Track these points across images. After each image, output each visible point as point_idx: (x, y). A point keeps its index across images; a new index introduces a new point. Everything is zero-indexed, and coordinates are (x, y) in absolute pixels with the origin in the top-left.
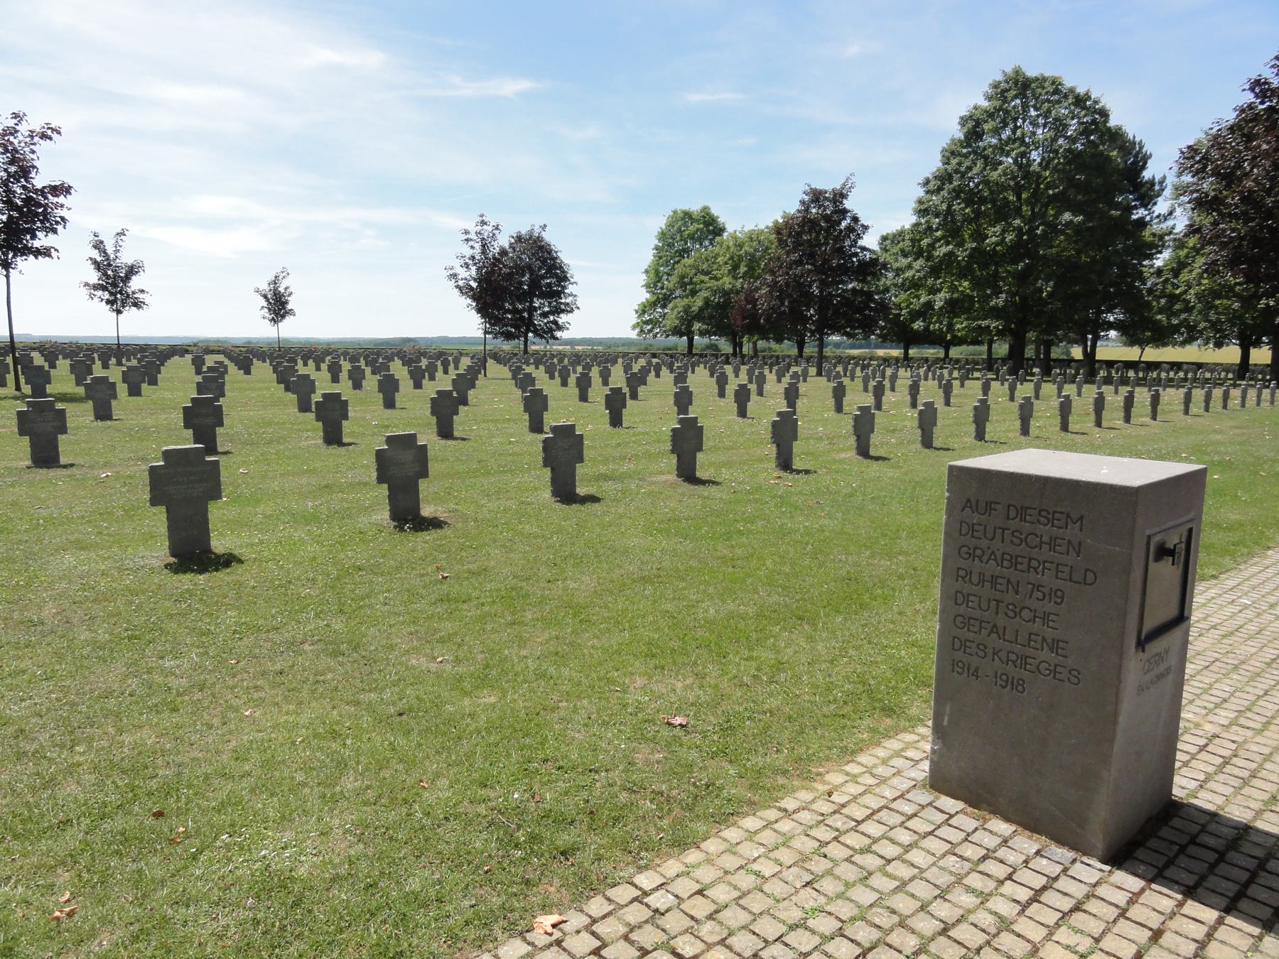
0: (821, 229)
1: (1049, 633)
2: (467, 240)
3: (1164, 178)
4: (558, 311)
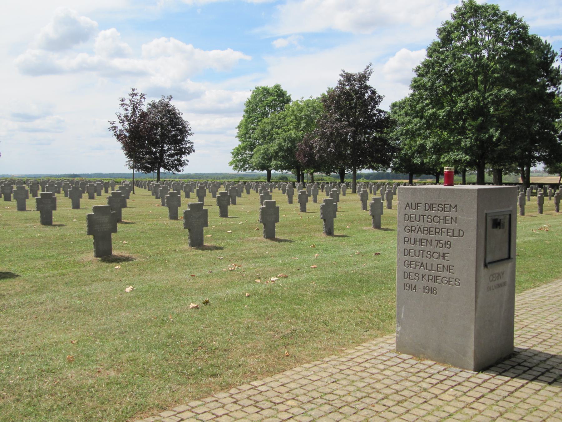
0: (353, 98)
1: (446, 263)
2: (122, 105)
4: (182, 152)
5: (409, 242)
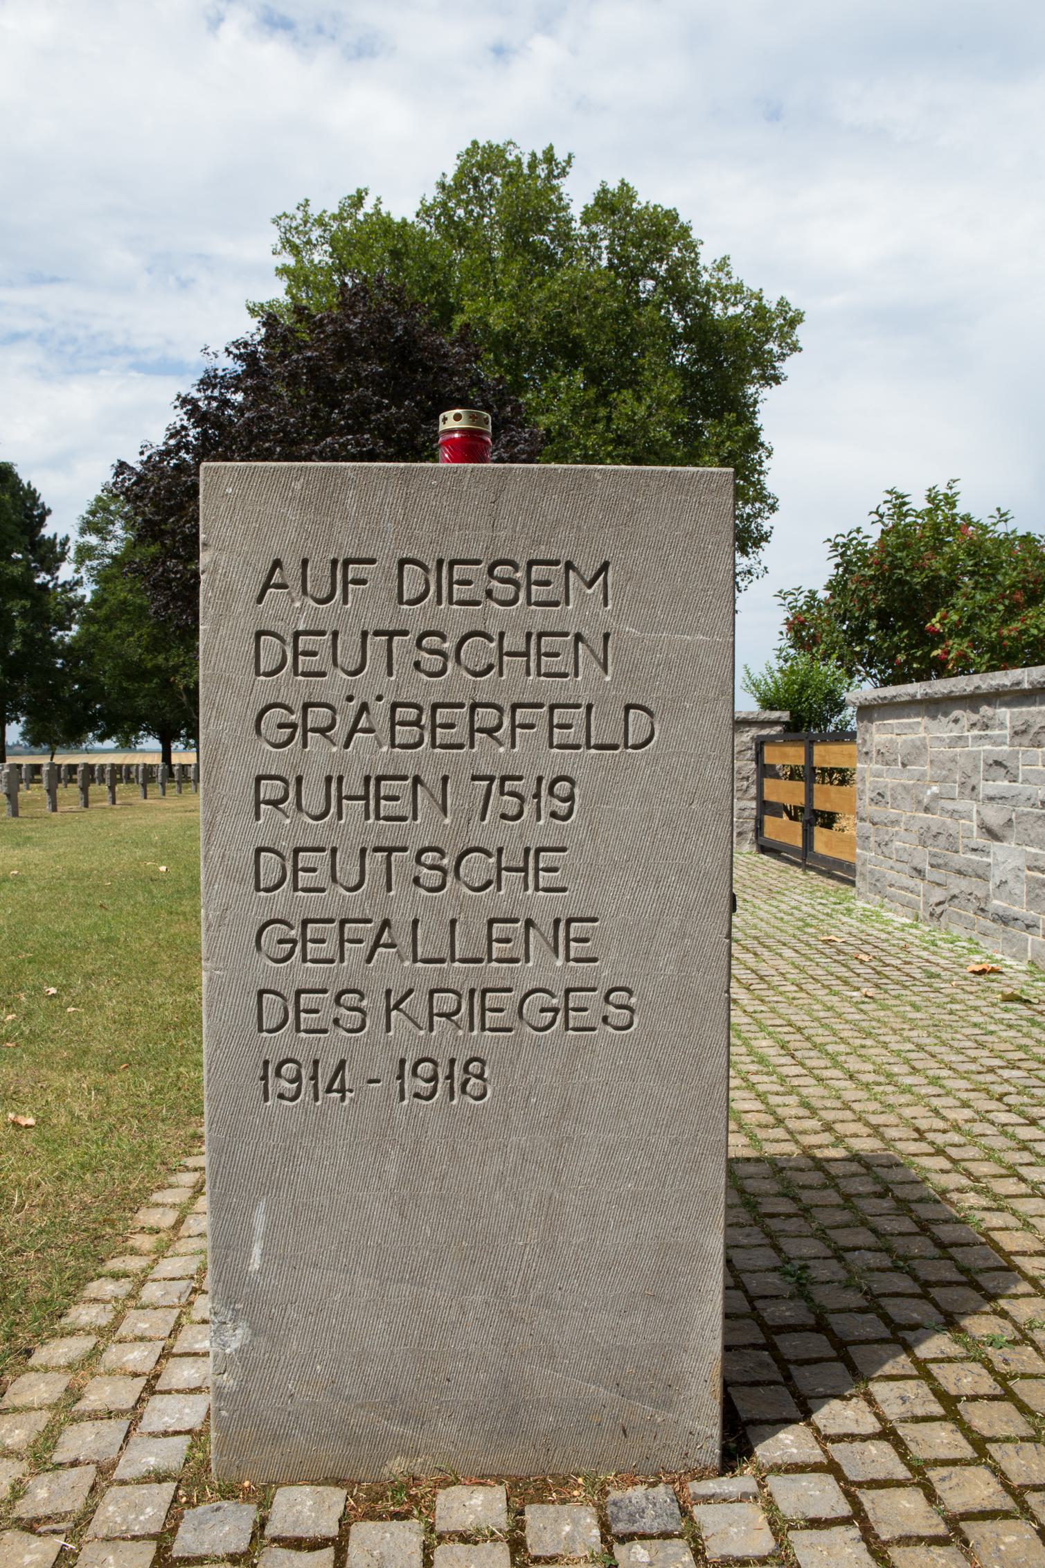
1: (543, 907)
3: (67, 539)
5: (289, 805)
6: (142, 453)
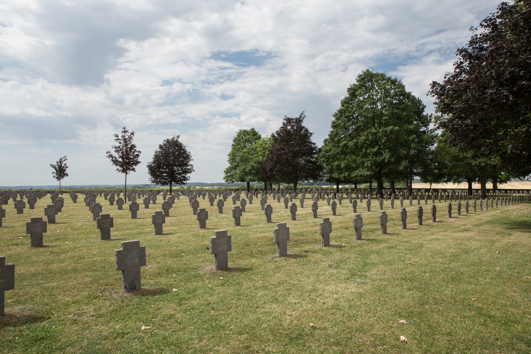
0: (293, 135)
3: (432, 114)
4: (186, 172)
6: (445, 78)
